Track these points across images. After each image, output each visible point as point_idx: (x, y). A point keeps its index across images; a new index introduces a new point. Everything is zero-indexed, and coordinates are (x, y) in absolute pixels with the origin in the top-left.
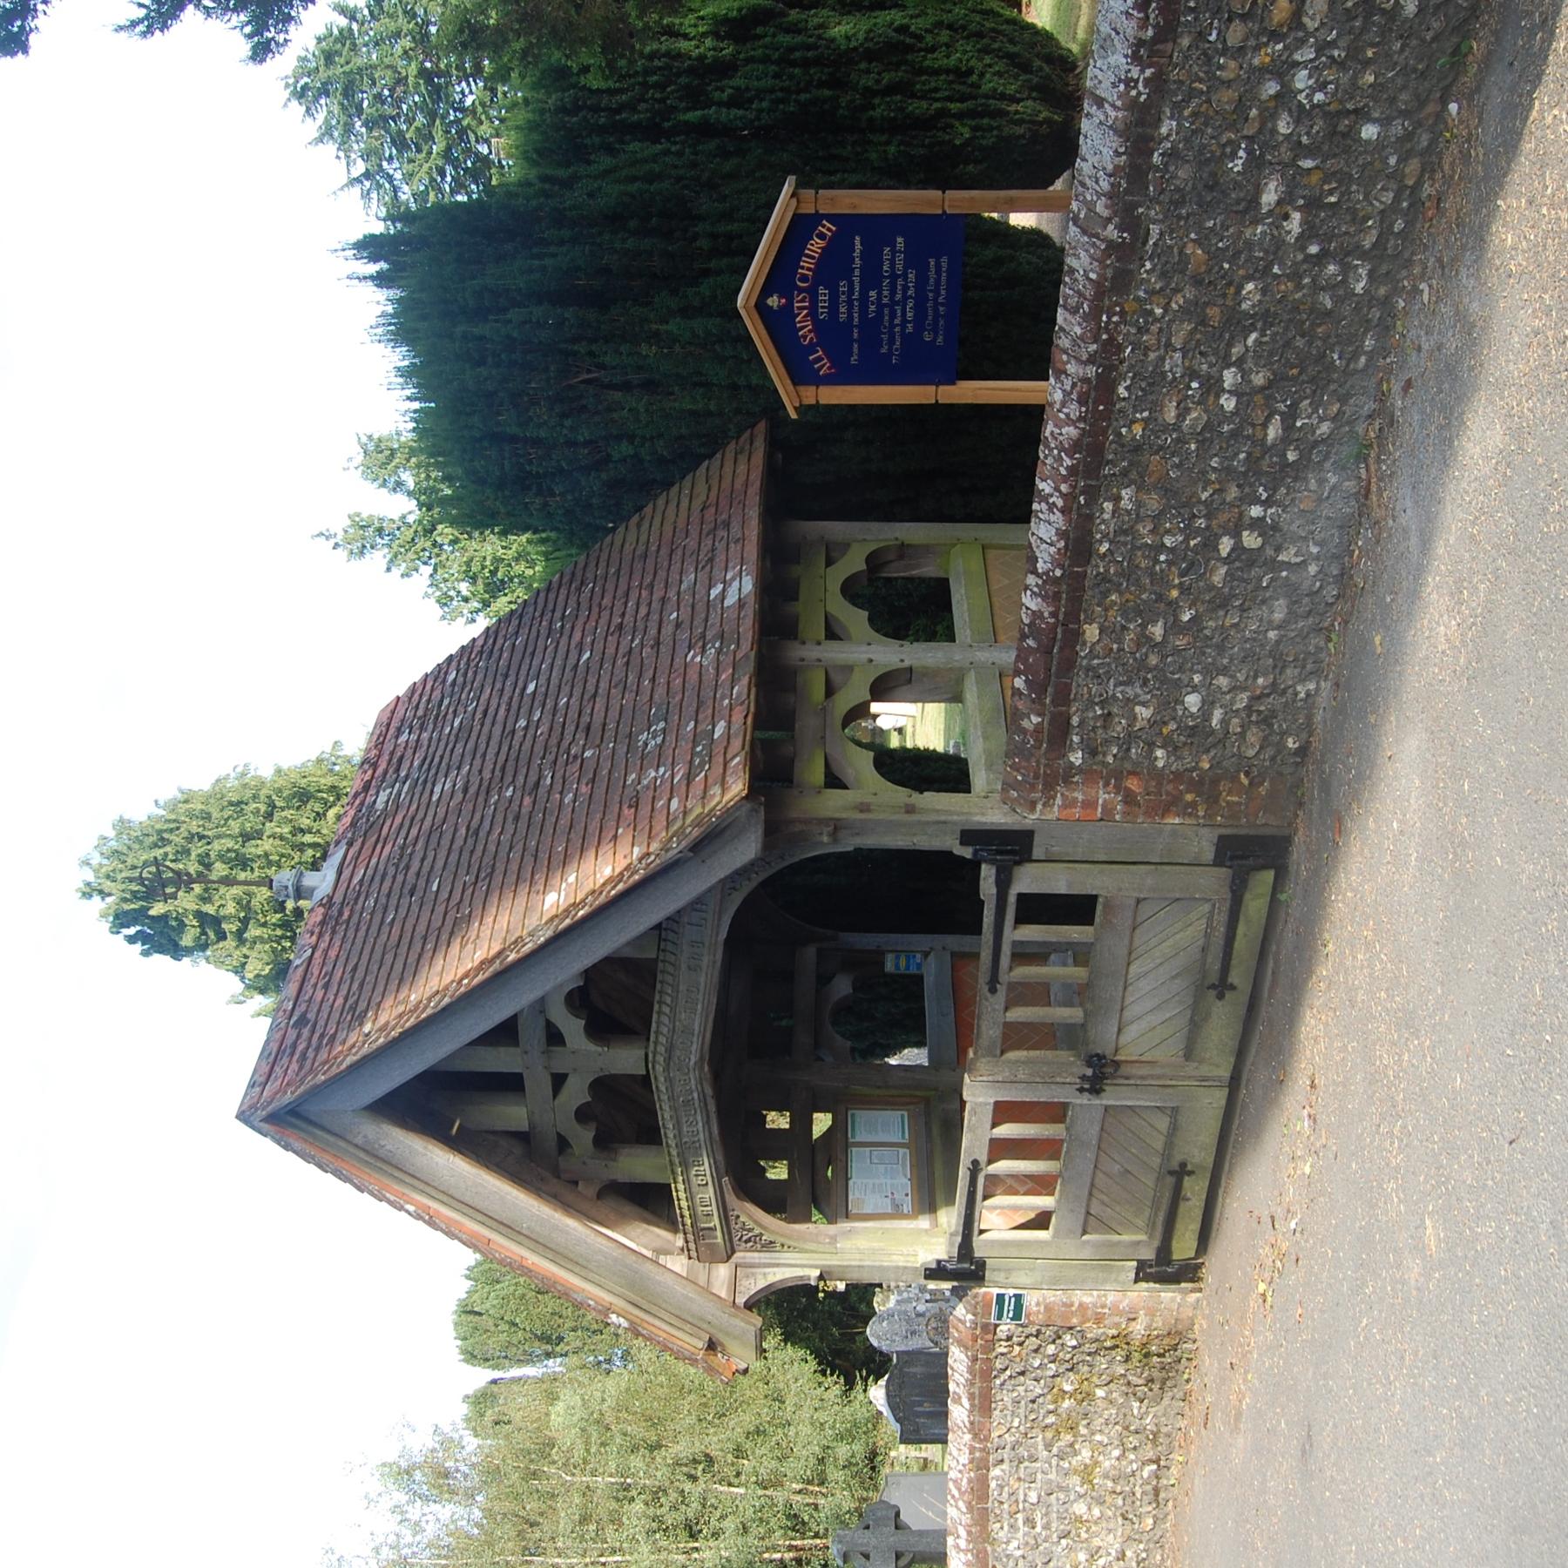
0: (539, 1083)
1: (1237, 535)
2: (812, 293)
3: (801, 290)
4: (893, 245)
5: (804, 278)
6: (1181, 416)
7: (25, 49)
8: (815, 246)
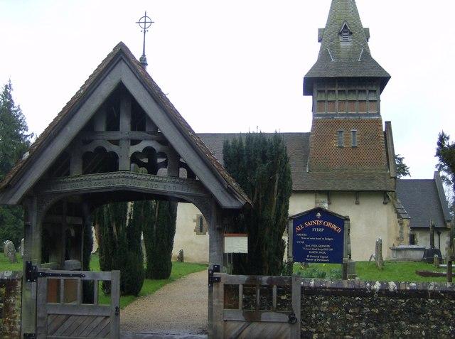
0: (113, 135)
1: (316, 332)
2: (321, 226)
3: (323, 223)
4: (331, 248)
5: (326, 224)
6: (351, 314)
7: (368, 29)
8: (335, 227)
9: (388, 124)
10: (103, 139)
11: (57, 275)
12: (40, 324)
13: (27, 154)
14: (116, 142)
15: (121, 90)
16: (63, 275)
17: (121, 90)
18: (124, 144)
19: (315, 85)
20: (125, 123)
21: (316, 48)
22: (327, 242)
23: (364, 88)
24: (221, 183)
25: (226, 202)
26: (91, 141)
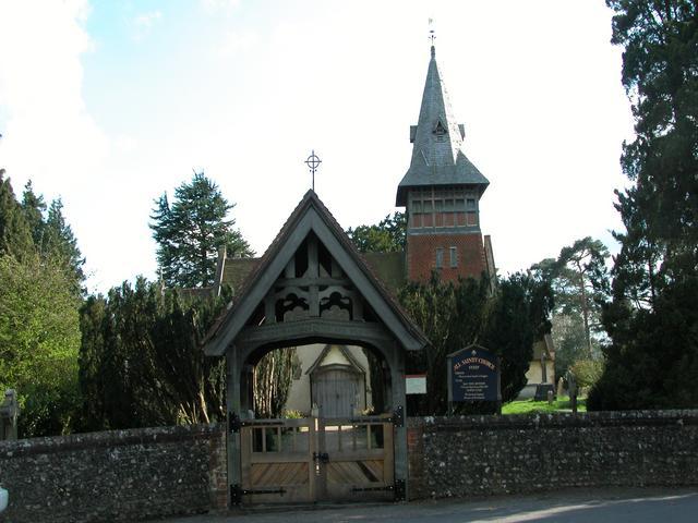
9: (488, 237)
10: (292, 287)
11: (259, 424)
12: (244, 475)
13: (231, 304)
14: (306, 289)
15: (312, 236)
16: (264, 424)
17: (312, 236)
18: (313, 290)
19: (410, 194)
20: (313, 268)
21: (408, 149)
22: (482, 380)
23: (461, 197)
24: (404, 326)
25: (411, 345)
26: (283, 288)
